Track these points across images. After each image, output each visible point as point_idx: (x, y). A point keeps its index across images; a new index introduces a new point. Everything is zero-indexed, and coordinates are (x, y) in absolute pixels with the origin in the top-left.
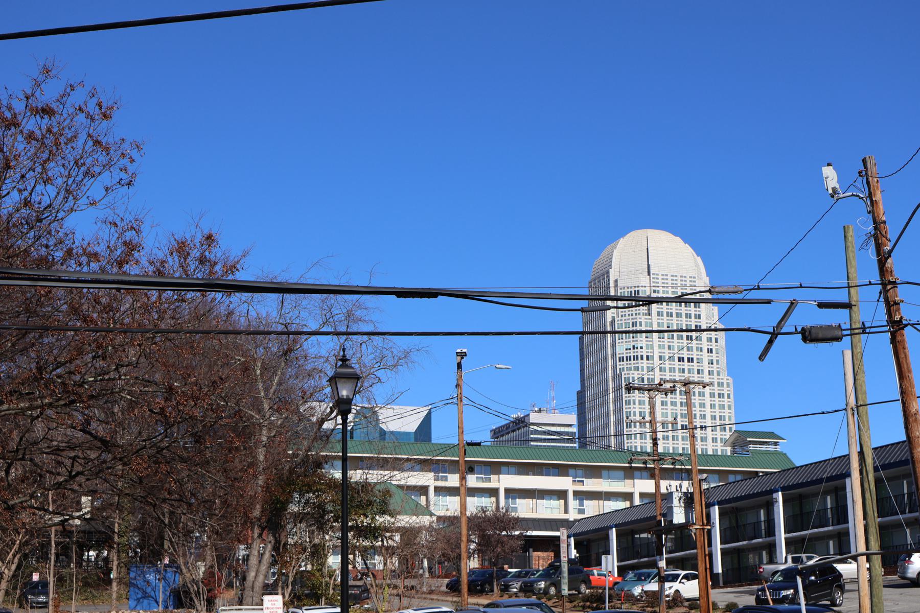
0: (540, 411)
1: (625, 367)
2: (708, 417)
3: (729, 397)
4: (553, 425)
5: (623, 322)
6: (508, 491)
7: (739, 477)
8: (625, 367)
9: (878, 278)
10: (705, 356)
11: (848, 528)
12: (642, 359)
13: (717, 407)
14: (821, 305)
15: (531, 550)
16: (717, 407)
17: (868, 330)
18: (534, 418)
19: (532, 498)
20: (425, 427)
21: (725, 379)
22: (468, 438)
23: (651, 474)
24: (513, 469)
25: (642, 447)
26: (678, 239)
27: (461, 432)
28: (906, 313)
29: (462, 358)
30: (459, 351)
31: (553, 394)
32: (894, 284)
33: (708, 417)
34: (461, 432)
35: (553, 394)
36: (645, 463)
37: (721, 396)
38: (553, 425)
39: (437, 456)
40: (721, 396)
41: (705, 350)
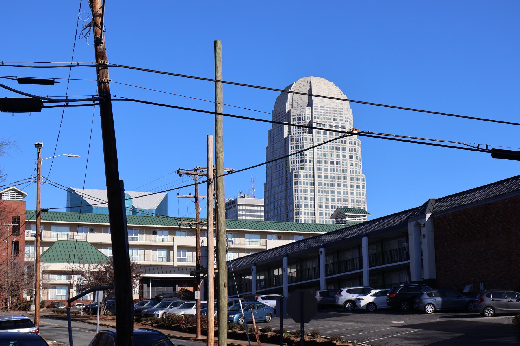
0: (244, 197)
1: (295, 167)
2: (349, 201)
3: (363, 187)
4: (253, 206)
5: (294, 138)
6: (180, 248)
7: (302, 238)
8: (295, 167)
9: (94, 60)
10: (348, 161)
11: (362, 272)
12: (306, 162)
13: (355, 194)
14: (51, 82)
15: (177, 285)
16: (355, 194)
17: (70, 103)
18: (240, 201)
19: (149, 249)
20: (163, 206)
21: (361, 176)
22: (43, 206)
23: (191, 232)
24: (275, 236)
25: (305, 220)
26: (332, 83)
27: (38, 202)
28: (114, 91)
29: (40, 149)
30: (37, 143)
31: (253, 185)
32: (105, 66)
33: (349, 201)
34: (38, 202)
35: (253, 185)
36: (190, 226)
37: (358, 187)
38: (253, 206)
39: (30, 219)
40: (358, 187)
41: (348, 157)
